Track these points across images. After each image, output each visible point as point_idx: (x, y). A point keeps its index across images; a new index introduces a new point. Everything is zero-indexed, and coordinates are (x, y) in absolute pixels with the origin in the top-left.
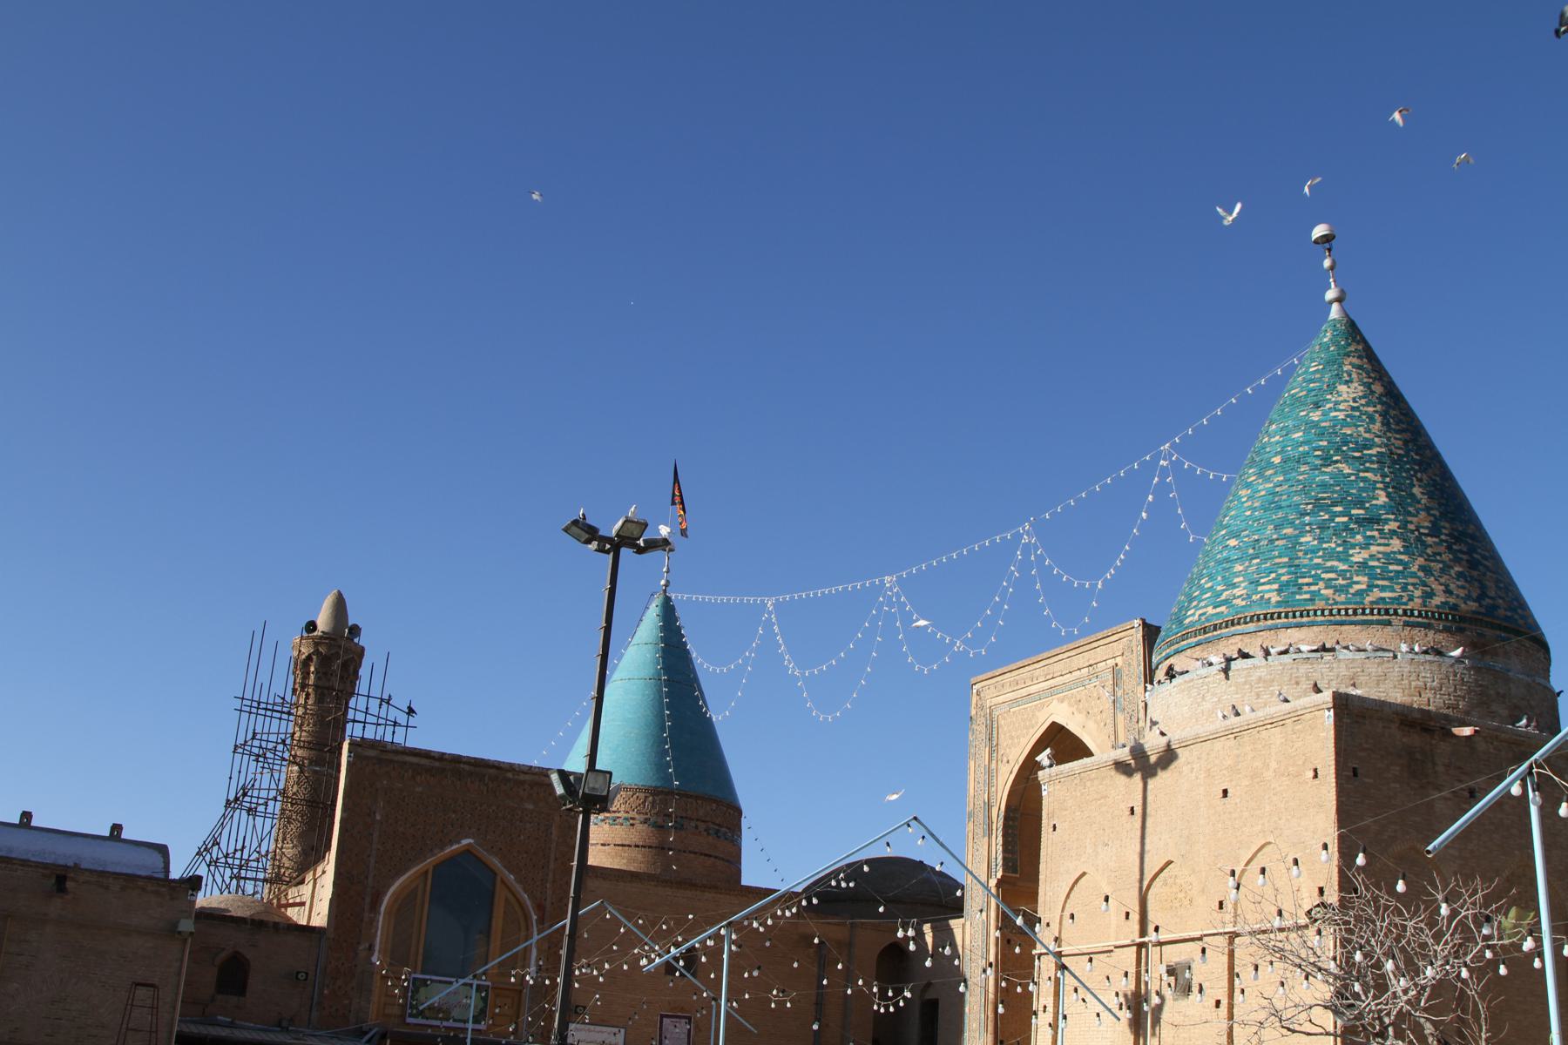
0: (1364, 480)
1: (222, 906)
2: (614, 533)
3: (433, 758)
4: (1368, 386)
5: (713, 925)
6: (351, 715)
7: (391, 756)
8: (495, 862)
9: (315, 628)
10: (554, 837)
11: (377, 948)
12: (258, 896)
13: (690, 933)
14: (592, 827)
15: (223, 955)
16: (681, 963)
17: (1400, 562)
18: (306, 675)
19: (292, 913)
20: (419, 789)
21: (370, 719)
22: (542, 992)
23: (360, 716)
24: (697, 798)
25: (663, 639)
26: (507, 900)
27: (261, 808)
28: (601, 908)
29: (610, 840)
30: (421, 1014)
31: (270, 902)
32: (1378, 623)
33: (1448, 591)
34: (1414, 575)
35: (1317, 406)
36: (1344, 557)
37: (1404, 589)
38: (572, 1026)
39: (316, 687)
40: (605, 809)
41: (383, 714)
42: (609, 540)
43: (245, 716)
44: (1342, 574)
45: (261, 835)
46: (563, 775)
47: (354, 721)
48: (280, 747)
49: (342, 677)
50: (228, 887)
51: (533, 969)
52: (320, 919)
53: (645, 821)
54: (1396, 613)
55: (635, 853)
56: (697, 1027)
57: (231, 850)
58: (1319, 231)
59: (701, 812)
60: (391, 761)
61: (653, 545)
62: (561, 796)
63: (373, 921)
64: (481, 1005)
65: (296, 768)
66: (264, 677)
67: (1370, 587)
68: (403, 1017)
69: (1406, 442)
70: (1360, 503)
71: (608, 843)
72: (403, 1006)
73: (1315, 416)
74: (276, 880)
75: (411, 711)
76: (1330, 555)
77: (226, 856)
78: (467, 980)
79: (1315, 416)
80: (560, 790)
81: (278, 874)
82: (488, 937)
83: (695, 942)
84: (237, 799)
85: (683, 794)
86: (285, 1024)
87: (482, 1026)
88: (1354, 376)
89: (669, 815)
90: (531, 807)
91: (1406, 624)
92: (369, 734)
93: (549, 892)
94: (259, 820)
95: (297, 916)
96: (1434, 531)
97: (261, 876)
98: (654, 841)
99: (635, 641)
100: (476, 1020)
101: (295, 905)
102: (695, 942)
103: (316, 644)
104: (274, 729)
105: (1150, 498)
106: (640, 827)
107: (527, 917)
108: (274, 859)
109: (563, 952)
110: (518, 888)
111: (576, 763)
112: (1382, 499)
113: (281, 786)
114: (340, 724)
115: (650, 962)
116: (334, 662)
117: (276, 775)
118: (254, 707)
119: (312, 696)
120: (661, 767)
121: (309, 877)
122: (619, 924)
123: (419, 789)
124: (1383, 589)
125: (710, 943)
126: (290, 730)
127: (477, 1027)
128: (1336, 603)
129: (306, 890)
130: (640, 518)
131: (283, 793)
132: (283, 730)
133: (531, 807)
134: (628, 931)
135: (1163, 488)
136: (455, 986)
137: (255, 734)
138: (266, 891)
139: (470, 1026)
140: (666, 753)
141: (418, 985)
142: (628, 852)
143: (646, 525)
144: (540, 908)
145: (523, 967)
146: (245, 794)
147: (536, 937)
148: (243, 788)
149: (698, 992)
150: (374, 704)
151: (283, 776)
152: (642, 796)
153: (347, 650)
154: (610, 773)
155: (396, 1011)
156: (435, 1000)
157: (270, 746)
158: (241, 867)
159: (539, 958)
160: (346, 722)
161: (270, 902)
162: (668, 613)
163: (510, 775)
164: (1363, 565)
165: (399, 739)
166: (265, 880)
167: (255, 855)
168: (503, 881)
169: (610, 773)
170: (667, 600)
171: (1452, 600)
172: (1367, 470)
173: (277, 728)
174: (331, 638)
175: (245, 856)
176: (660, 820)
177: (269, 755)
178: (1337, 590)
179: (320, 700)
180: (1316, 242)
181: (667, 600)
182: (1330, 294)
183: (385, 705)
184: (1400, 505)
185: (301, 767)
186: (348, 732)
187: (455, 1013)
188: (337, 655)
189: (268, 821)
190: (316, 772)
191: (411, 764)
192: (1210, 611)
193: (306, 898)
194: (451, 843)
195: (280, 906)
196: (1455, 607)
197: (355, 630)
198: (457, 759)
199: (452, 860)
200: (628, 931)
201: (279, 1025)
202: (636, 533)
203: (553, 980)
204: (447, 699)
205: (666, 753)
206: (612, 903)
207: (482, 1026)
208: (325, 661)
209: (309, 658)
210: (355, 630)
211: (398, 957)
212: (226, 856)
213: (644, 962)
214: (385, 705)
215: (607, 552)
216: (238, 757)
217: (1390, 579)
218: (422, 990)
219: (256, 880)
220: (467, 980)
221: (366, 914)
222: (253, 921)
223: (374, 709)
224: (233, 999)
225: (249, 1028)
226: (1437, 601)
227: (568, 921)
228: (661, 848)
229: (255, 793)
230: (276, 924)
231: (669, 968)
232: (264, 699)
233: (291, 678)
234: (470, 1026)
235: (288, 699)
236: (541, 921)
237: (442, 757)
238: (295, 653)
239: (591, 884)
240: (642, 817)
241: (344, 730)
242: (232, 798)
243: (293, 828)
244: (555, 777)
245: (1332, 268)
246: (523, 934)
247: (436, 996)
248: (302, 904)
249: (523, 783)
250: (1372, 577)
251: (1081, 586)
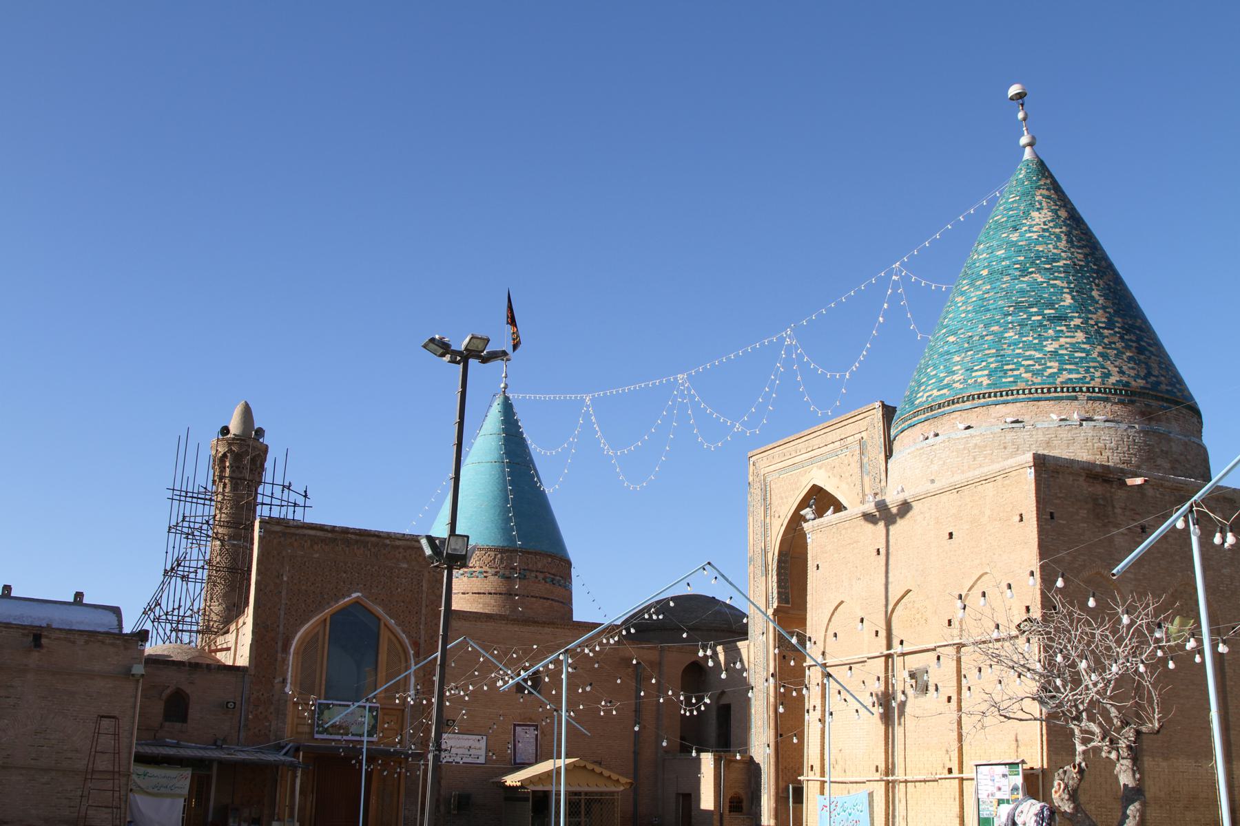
0: (1054, 286)
4: (1055, 212)
17: (1083, 350)
21: (275, 502)
27: (192, 575)
32: (1068, 398)
33: (1121, 372)
34: (1094, 360)
35: (1015, 229)
36: (1038, 347)
37: (1087, 371)
44: (1038, 361)
54: (1081, 390)
58: (1014, 90)
67: (1061, 370)
69: (1086, 256)
70: (1051, 305)
73: (1014, 237)
76: (1028, 346)
79: (1014, 237)
88: (1044, 204)
91: (1089, 399)
96: (1110, 325)
105: (886, 306)
112: (1068, 301)
116: (244, 458)
124: (1070, 371)
128: (1034, 384)
135: (895, 298)
150: (278, 491)
164: (1055, 353)
171: (1125, 379)
172: (1056, 279)
178: (1035, 373)
180: (1011, 99)
182: (1024, 140)
184: (1082, 306)
192: (935, 393)
196: (1127, 384)
216: (172, 535)
217: (1076, 364)
223: (278, 493)
226: (1113, 380)
245: (1025, 119)
250: (1062, 362)
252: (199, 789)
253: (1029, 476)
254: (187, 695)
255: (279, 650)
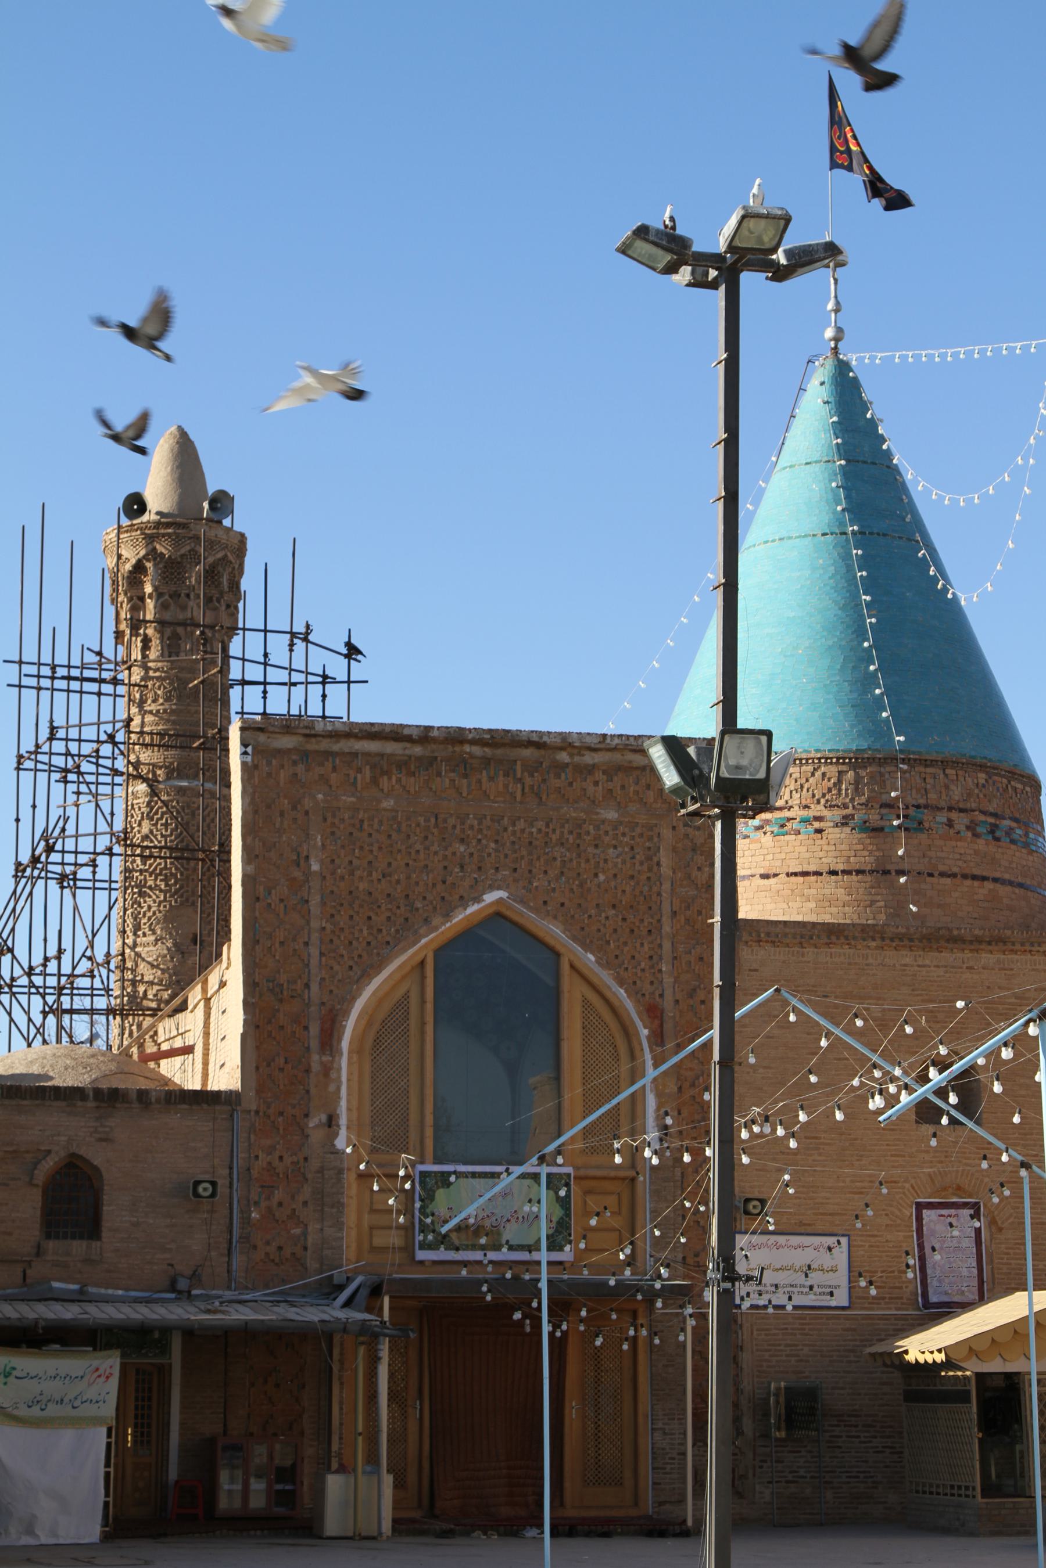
1: (35, 1069)
2: (722, 246)
3: (409, 739)
5: (1009, 1017)
6: (235, 671)
7: (325, 745)
8: (555, 932)
9: (143, 508)
10: (665, 870)
11: (343, 1121)
12: (100, 1044)
13: (967, 1033)
14: (741, 844)
15: (49, 1164)
16: (953, 1099)
18: (138, 602)
19: (170, 1069)
20: (388, 804)
21: (274, 675)
22: (676, 1178)
23: (254, 673)
24: (944, 764)
25: (843, 451)
26: (586, 1003)
27: (85, 873)
28: (778, 1003)
29: (776, 866)
30: (443, 1240)
31: (126, 1053)
38: (741, 1240)
39: (161, 623)
40: (765, 806)
41: (299, 663)
42: (715, 260)
43: (29, 695)
45: (89, 924)
46: (674, 746)
47: (244, 683)
48: (106, 750)
49: (209, 600)
50: (40, 1030)
51: (652, 1135)
52: (226, 1074)
53: (845, 821)
55: (829, 886)
56: (992, 1222)
57: (37, 960)
59: (957, 793)
60: (328, 754)
61: (805, 259)
62: (676, 790)
63: (328, 1071)
64: (558, 1213)
65: (142, 787)
66: (55, 616)
68: (408, 1250)
71: (778, 872)
72: (407, 1230)
74: (130, 1008)
75: (352, 651)
77: (30, 972)
78: (527, 1168)
80: (670, 777)
81: (133, 997)
82: (558, 1078)
83: (977, 1057)
84: (35, 860)
85: (915, 761)
86: (182, 1284)
87: (567, 1254)
89: (890, 805)
90: (612, 815)
92: (277, 705)
93: (668, 980)
94: (84, 897)
95: (182, 1074)
97: (101, 1003)
98: (866, 861)
99: (785, 459)
100: (554, 1245)
101: (172, 1053)
102: (977, 1057)
103: (150, 539)
104: (90, 716)
106: (833, 834)
107: (628, 1032)
108: (122, 968)
109: (712, 1097)
110: (605, 977)
111: (697, 719)
113: (118, 825)
114: (217, 693)
115: (893, 1099)
116: (188, 572)
117: (105, 805)
118: (52, 676)
119: (155, 643)
120: (863, 709)
121: (195, 995)
122: (817, 1031)
123: (388, 804)
125: (1006, 1054)
126: (122, 715)
127: (557, 1256)
129: (191, 1021)
130: (773, 205)
131: (125, 838)
132: (107, 715)
133: (612, 815)
134: (836, 1044)
136: (505, 1181)
137: (53, 729)
138: (115, 1031)
139: (544, 1256)
140: (870, 680)
141: (432, 1184)
142: (815, 887)
143: (787, 220)
144: (653, 1012)
145: (633, 1134)
146: (50, 849)
147: (651, 1073)
148: (45, 836)
149: (988, 1153)
150: (278, 645)
151: (120, 807)
152: (832, 771)
153: (211, 544)
154: (769, 734)
155: (395, 1239)
156: (470, 1212)
157: (87, 749)
158: (60, 990)
159: (660, 1117)
160: (227, 686)
161: (126, 1053)
162: (847, 392)
163: (564, 757)
165: (336, 708)
166: (110, 1011)
167: (84, 966)
168: (572, 966)
169: (769, 734)
170: (842, 368)
173: (97, 712)
174: (176, 525)
175: (66, 969)
176: (874, 817)
177: (85, 767)
179: (171, 647)
181: (842, 368)
183: (300, 645)
185: (152, 783)
186: (235, 706)
187: (510, 1233)
188: (194, 557)
189: (102, 896)
190: (181, 791)
191: (367, 754)
193: (193, 1037)
194: (464, 901)
195: (145, 1058)
197: (222, 502)
198: (456, 737)
199: (467, 937)
200: (836, 1044)
201: (172, 1287)
202: (768, 242)
203: (698, 1154)
204: (413, 621)
205: (870, 680)
206: (795, 991)
207: (567, 1254)
208: (172, 570)
209: (139, 568)
210: (222, 502)
211: (387, 1134)
212: (30, 972)
213: (877, 1102)
214: (300, 645)
215: (713, 285)
216: (26, 777)
218: (440, 1194)
219: (92, 1012)
220: (527, 1168)
221: (315, 1057)
222: (98, 1092)
224: (78, 1247)
225: (122, 1300)
227: (715, 1033)
228: (883, 871)
229: (70, 845)
230: (142, 1095)
231: (926, 1112)
232: (61, 659)
233: (110, 611)
234: (544, 1256)
235: (108, 652)
236: (658, 1038)
237: (425, 735)
238: (111, 562)
239: (747, 955)
240: (837, 814)
241: (226, 703)
242: (25, 858)
243: (152, 903)
244: (658, 754)
246: (625, 1067)
247: (468, 1203)
248: (188, 1050)
249: (591, 769)
251: (954, 502)
252: (142, 1402)
253: (106, 1224)
254: (96, 1169)
255: (314, 1044)
